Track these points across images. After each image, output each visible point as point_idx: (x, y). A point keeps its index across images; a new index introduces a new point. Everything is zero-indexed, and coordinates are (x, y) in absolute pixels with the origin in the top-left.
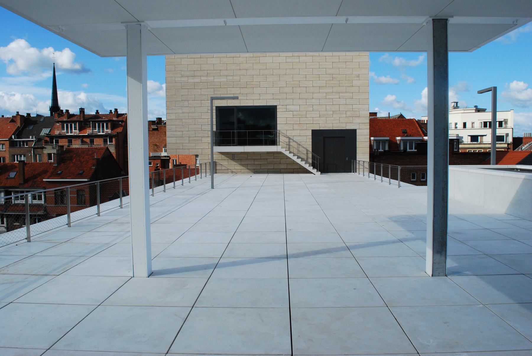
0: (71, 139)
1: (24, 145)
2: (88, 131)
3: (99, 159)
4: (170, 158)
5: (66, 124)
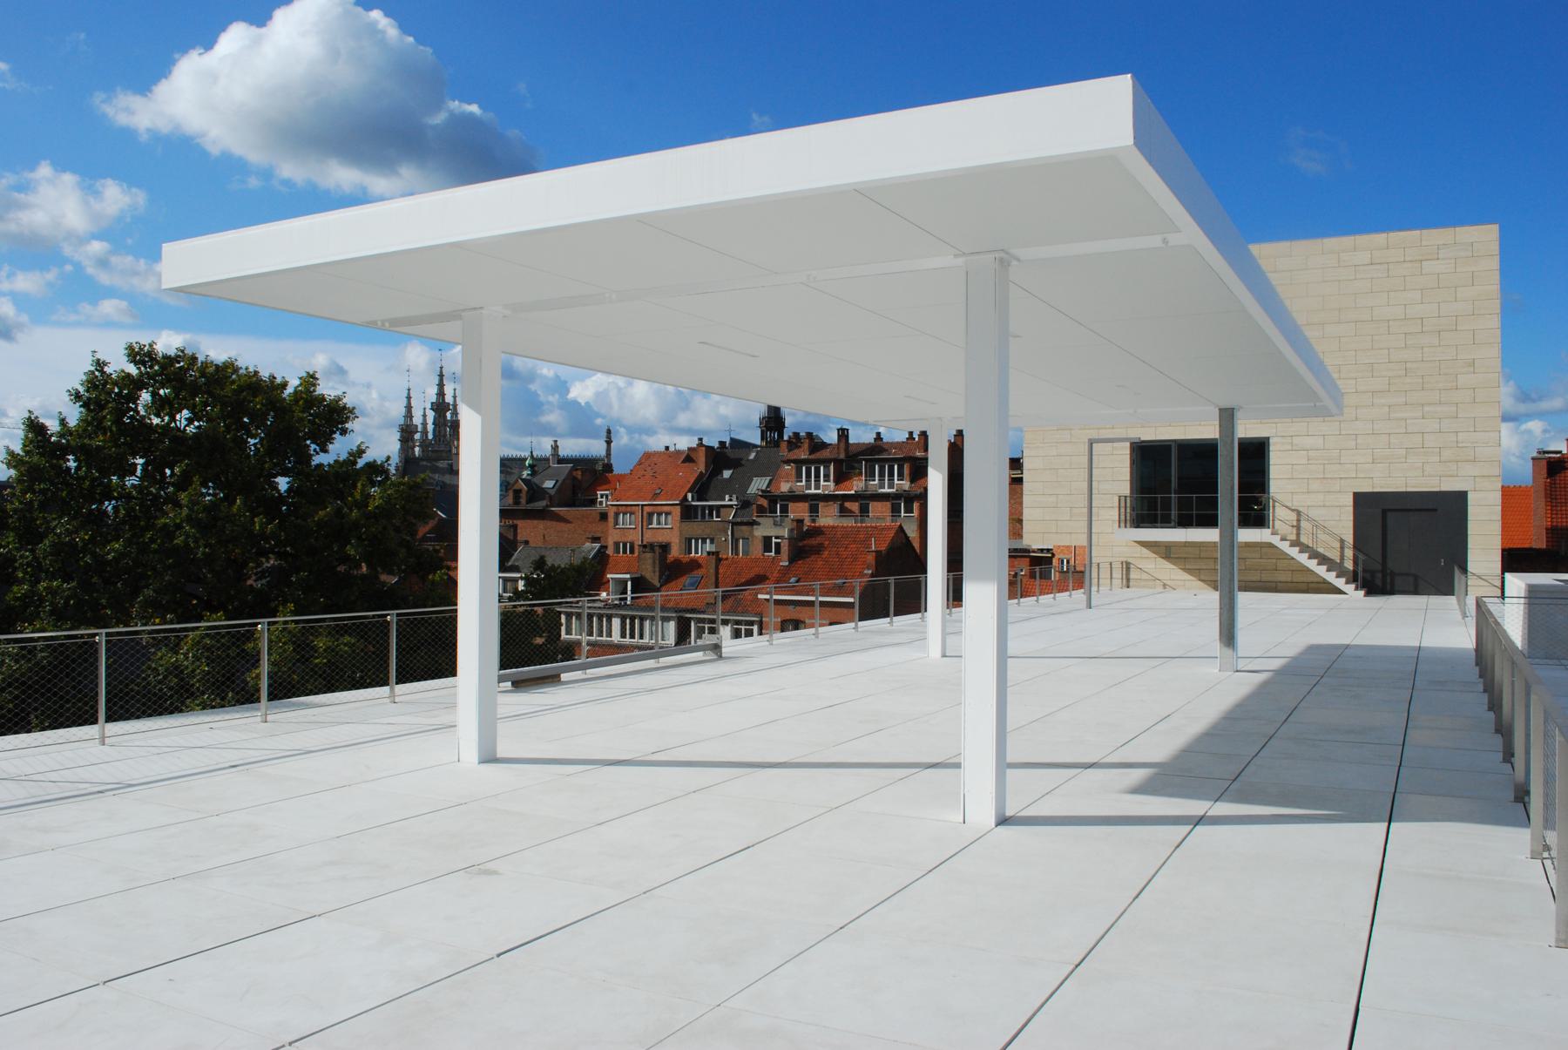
0: (816, 502)
1: (711, 515)
2: (856, 485)
3: (881, 551)
4: (1053, 555)
5: (806, 468)
